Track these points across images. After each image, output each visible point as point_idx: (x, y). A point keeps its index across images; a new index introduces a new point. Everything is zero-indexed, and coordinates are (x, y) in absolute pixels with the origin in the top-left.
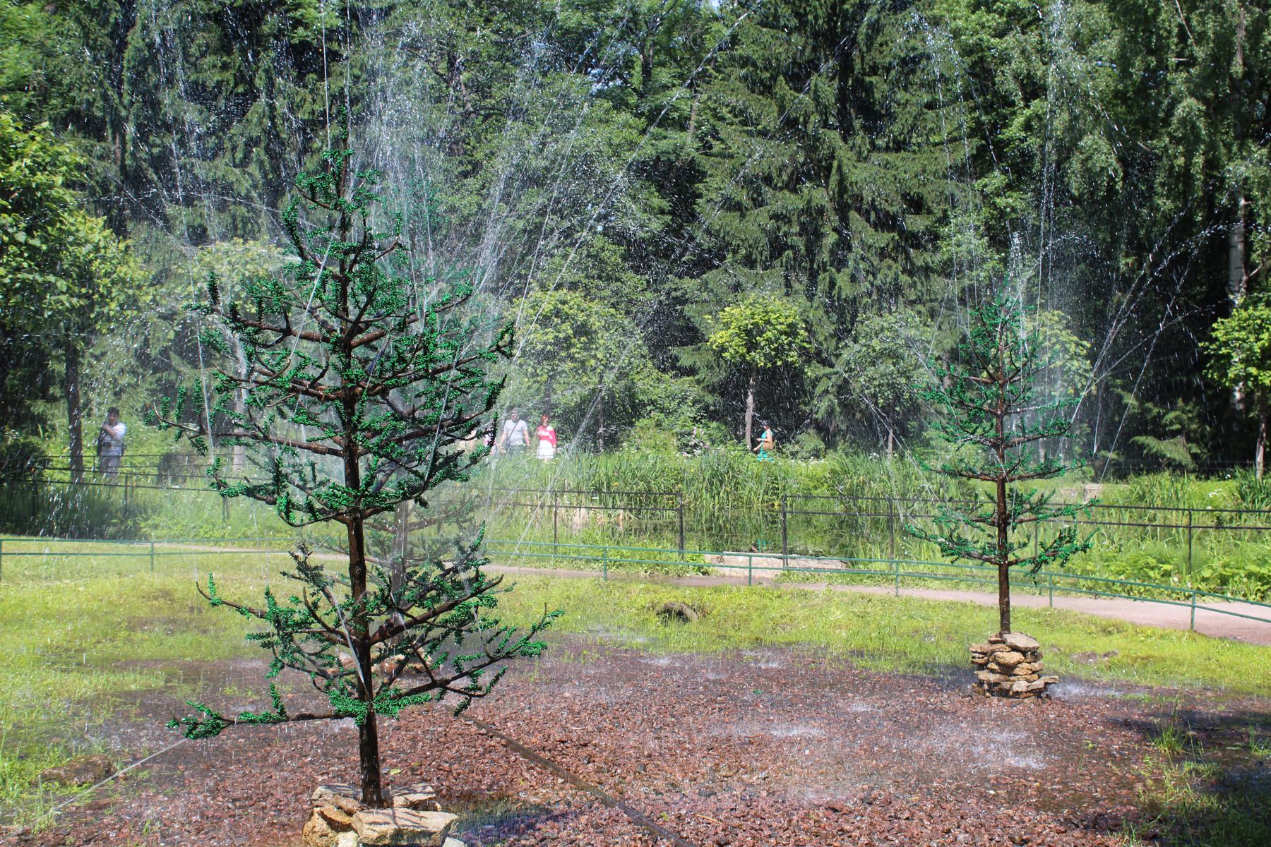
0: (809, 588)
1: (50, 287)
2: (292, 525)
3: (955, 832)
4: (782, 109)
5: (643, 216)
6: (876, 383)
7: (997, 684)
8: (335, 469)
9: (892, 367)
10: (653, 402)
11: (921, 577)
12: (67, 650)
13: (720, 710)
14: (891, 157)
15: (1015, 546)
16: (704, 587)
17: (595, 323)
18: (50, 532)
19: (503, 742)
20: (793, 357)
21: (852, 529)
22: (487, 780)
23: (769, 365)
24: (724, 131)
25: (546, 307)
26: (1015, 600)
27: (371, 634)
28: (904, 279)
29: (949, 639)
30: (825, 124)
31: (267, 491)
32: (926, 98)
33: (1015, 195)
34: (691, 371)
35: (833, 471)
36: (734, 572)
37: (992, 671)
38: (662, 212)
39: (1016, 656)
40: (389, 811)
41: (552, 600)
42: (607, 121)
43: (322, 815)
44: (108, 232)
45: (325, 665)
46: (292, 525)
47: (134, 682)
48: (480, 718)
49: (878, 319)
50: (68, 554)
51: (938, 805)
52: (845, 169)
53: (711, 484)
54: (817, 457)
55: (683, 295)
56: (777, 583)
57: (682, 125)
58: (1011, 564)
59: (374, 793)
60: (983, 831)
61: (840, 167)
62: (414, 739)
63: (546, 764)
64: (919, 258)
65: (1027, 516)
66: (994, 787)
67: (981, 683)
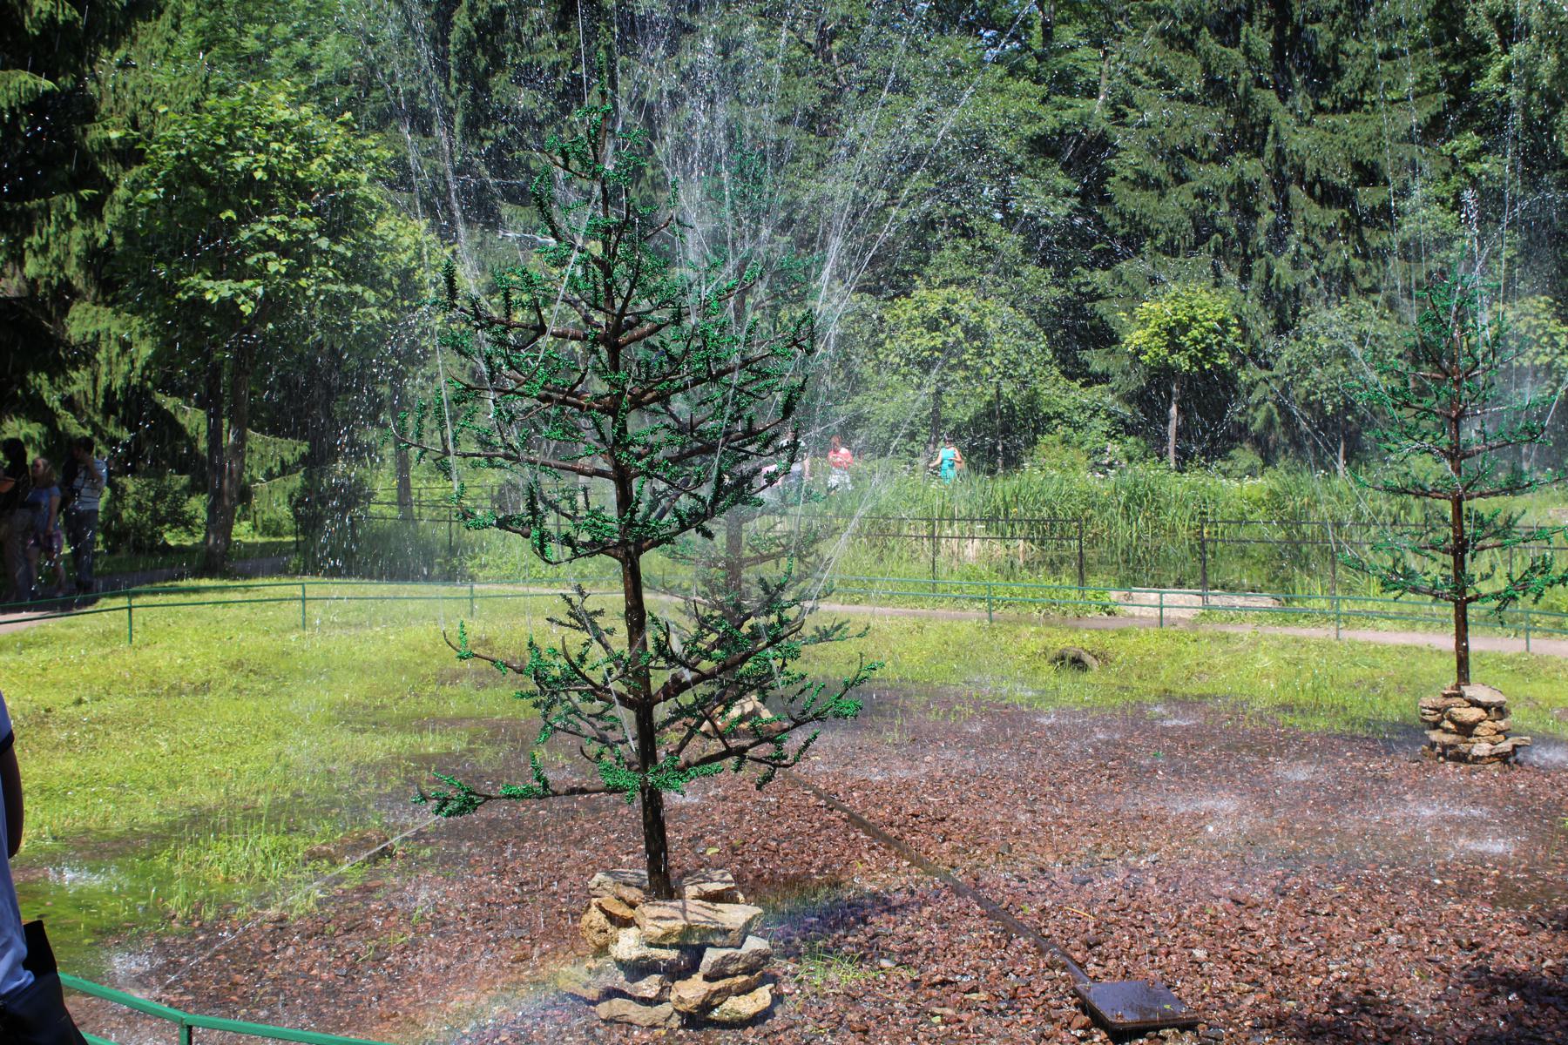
0: (1231, 630)
1: (354, 298)
2: (549, 562)
3: (1386, 932)
4: (1206, 67)
5: (1046, 197)
6: (1323, 387)
7: (1452, 746)
8: (605, 494)
9: (1342, 369)
10: (1059, 415)
11: (1369, 615)
12: (365, 707)
13: (1110, 777)
14: (1343, 120)
15: (1477, 578)
16: (1106, 629)
17: (991, 325)
18: (371, 577)
19: (844, 815)
20: (1224, 359)
21: (1292, 559)
22: (819, 862)
23: (1195, 369)
24: (1138, 95)
25: (934, 308)
26: (1475, 644)
27: (653, 692)
28: (1357, 264)
29: (1401, 691)
30: (1261, 84)
31: (521, 521)
32: (1380, 47)
33: (1491, 158)
34: (1104, 378)
35: (1272, 492)
36: (1145, 612)
37: (1446, 731)
38: (1068, 194)
39: (1477, 713)
40: (679, 903)
41: (928, 646)
42: (1001, 90)
43: (600, 907)
44: (432, 237)
45: (606, 729)
46: (549, 562)
47: (432, 744)
48: (822, 786)
49: (1324, 313)
50: (383, 599)
51: (1368, 897)
52: (1284, 136)
53: (1127, 508)
54: (1252, 475)
55: (1095, 290)
56: (1194, 625)
57: (1091, 92)
58: (1470, 600)
59: (663, 885)
60: (1422, 931)
61: (1276, 134)
62: (741, 812)
63: (891, 842)
64: (1375, 239)
65: (1490, 541)
66: (1441, 875)
67: (1433, 745)
